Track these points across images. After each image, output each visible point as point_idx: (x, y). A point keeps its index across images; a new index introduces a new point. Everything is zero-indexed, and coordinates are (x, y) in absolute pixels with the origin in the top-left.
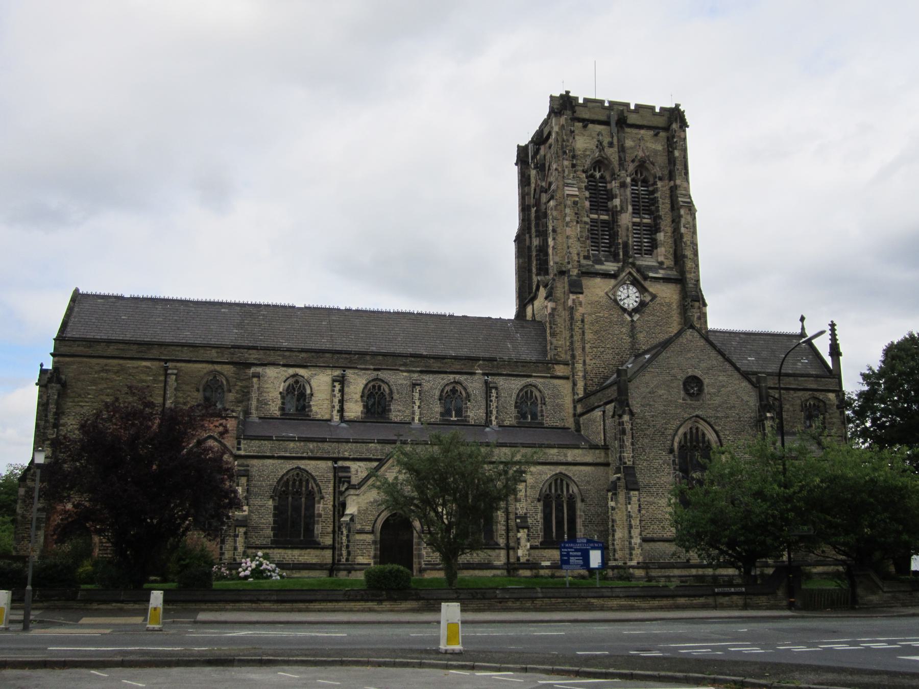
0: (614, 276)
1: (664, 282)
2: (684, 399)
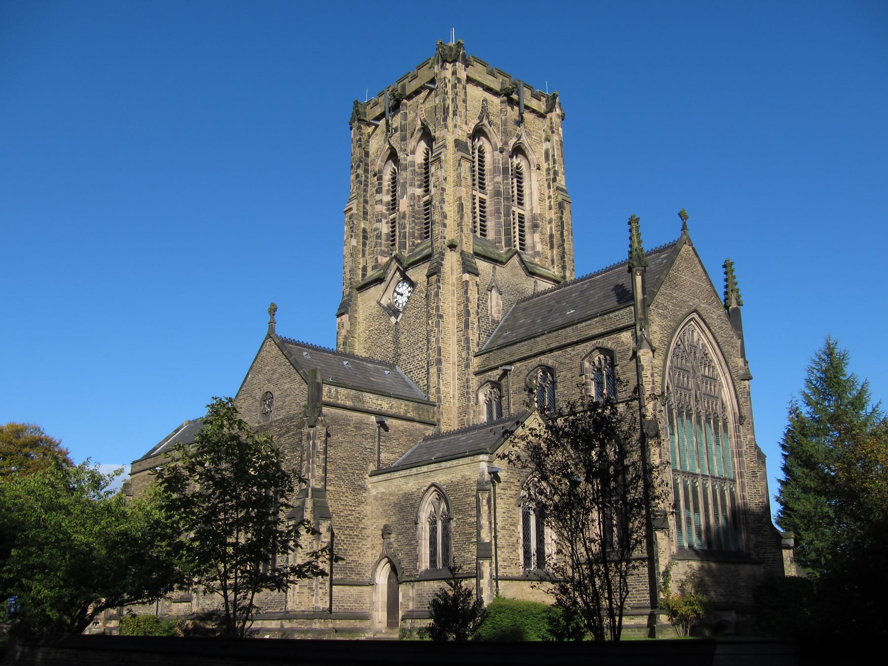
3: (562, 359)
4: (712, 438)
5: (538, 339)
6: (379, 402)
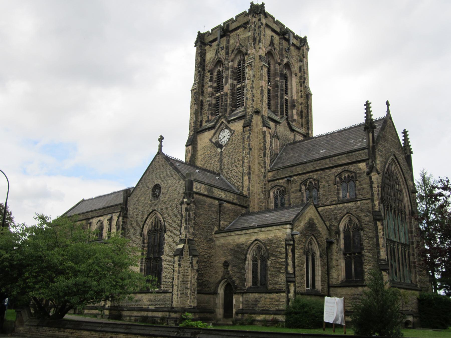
0: (212, 128)
1: (239, 120)
2: (151, 201)
3: (323, 176)
4: (400, 222)
5: (308, 164)
6: (220, 193)
